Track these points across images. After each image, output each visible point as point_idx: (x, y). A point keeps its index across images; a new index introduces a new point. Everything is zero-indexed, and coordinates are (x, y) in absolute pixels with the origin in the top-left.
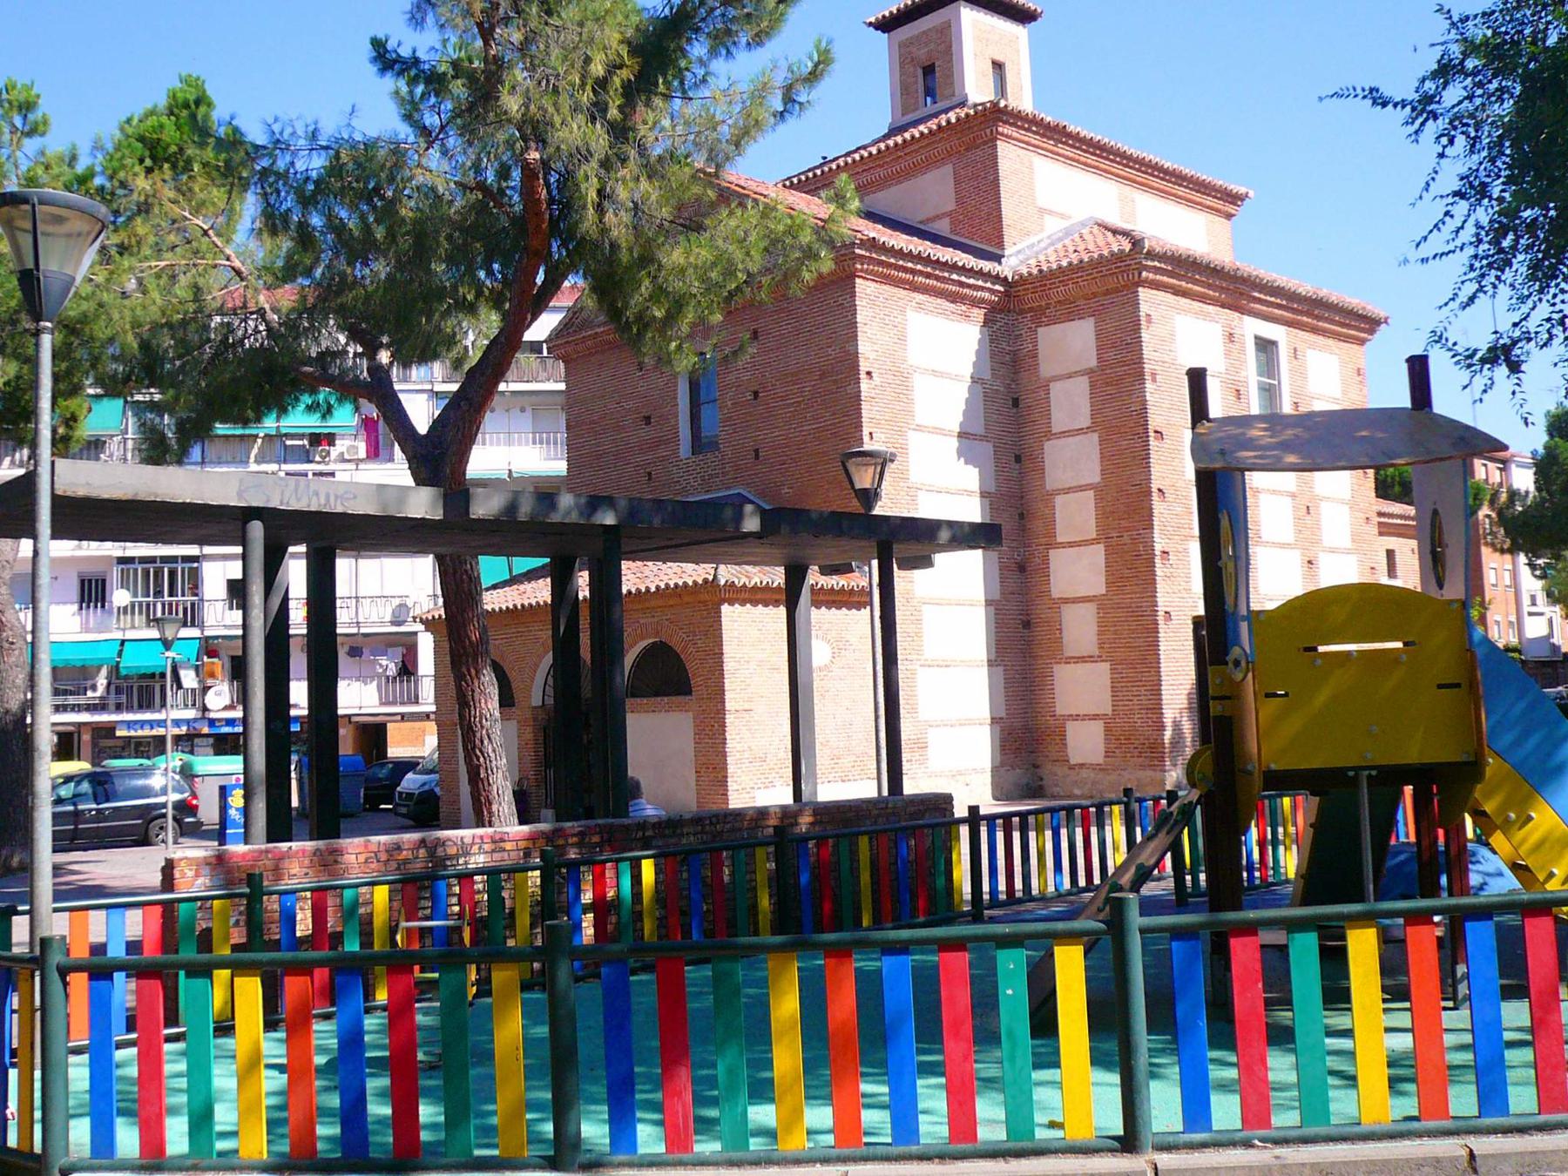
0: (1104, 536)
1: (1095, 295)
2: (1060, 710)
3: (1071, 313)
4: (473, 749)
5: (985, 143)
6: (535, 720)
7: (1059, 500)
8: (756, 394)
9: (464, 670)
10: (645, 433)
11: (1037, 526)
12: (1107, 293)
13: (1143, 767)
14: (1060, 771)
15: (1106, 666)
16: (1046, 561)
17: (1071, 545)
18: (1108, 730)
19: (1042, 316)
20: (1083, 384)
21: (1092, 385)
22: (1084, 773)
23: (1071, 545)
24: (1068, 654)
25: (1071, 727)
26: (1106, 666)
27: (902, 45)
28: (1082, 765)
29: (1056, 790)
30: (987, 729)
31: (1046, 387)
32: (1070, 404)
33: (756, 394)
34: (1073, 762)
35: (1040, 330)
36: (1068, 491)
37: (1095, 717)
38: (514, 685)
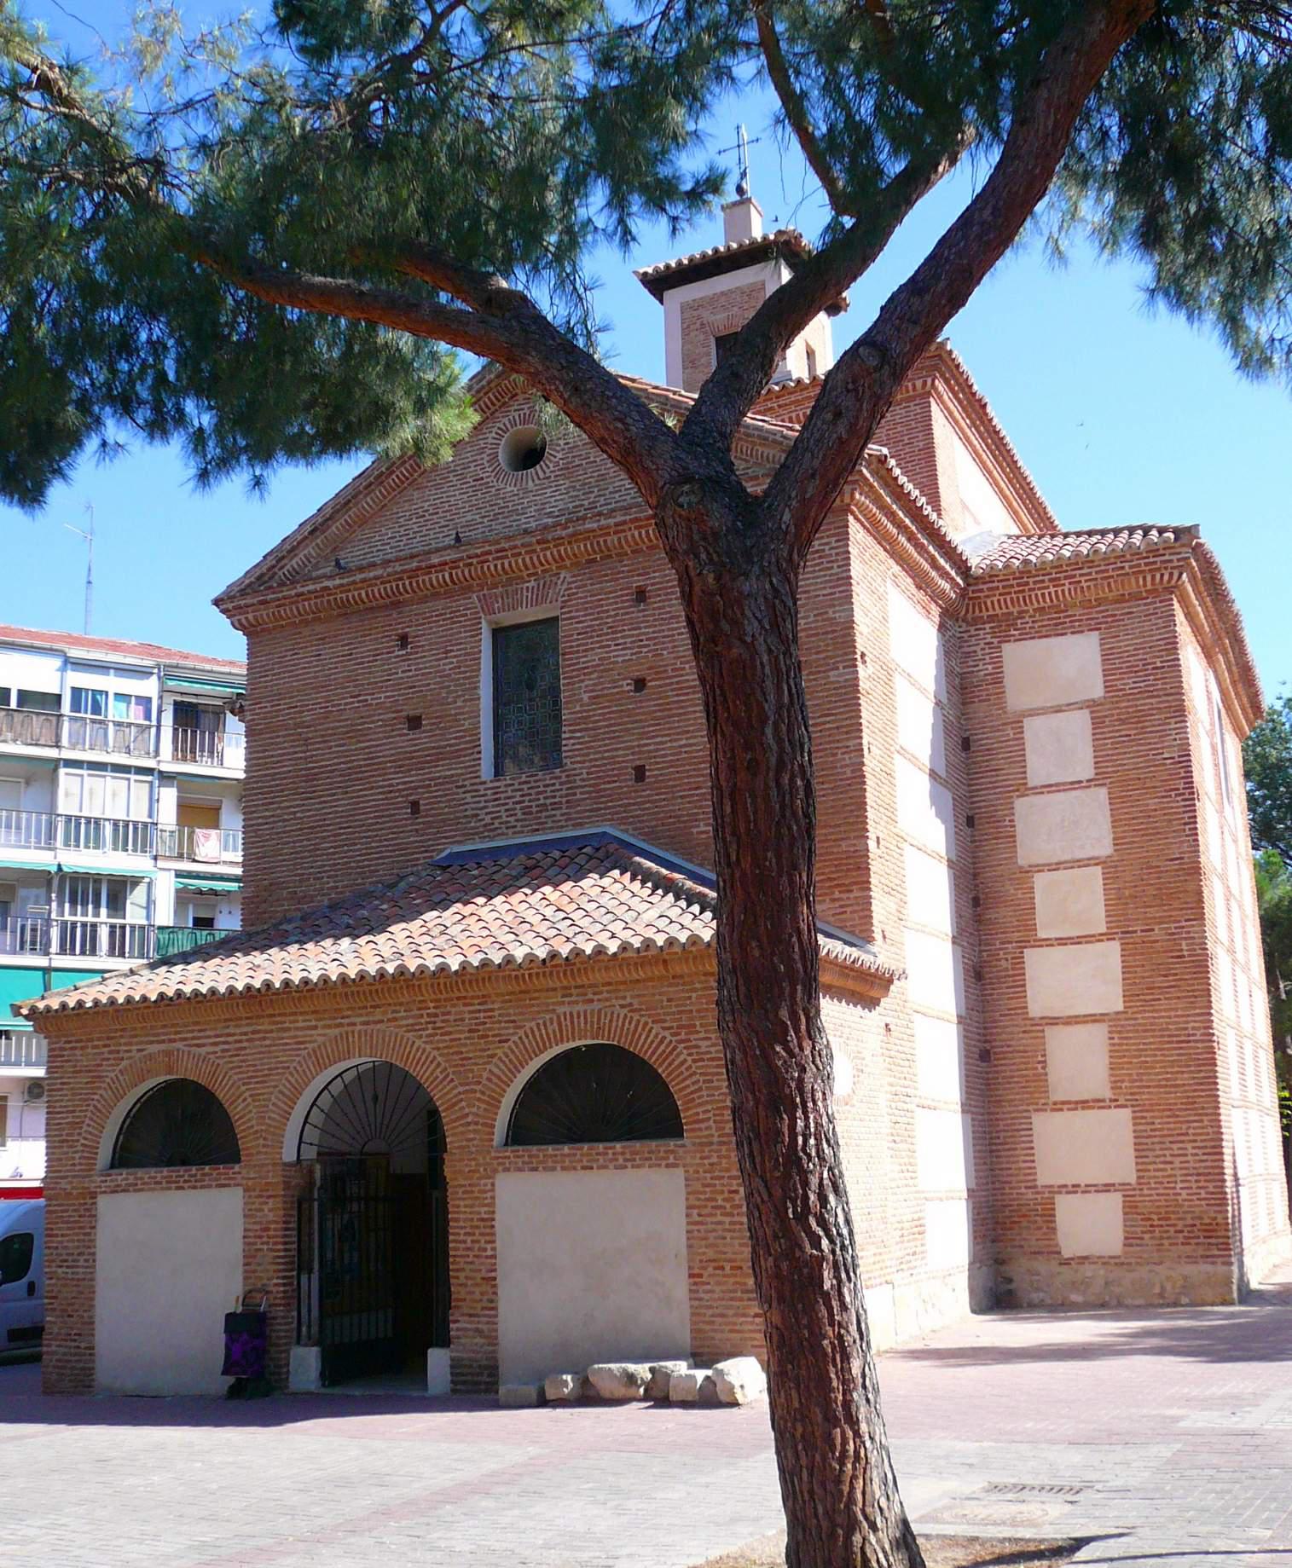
0: (1119, 927)
1: (1100, 602)
2: (1044, 1178)
3: (1058, 622)
4: (802, 1218)
5: (910, 399)
6: (287, 1185)
7: (1040, 881)
8: (640, 684)
9: (784, 1014)
10: (405, 741)
11: (1002, 915)
12: (1121, 599)
13: (1192, 1259)
14: (1042, 1266)
15: (1125, 1114)
16: (1019, 962)
17: (1062, 942)
18: (1130, 1208)
19: (1008, 627)
20: (1081, 722)
21: (1097, 723)
22: (1088, 1270)
23: (1062, 942)
24: (1057, 1095)
25: (1065, 1206)
26: (1125, 1114)
27: (685, 308)
28: (1084, 1259)
29: (1036, 1297)
30: (964, 1203)
31: (1017, 724)
32: (1058, 747)
33: (640, 684)
34: (1066, 1253)
35: (1005, 646)
36: (1056, 867)
37: (1107, 1188)
38: (239, 1128)
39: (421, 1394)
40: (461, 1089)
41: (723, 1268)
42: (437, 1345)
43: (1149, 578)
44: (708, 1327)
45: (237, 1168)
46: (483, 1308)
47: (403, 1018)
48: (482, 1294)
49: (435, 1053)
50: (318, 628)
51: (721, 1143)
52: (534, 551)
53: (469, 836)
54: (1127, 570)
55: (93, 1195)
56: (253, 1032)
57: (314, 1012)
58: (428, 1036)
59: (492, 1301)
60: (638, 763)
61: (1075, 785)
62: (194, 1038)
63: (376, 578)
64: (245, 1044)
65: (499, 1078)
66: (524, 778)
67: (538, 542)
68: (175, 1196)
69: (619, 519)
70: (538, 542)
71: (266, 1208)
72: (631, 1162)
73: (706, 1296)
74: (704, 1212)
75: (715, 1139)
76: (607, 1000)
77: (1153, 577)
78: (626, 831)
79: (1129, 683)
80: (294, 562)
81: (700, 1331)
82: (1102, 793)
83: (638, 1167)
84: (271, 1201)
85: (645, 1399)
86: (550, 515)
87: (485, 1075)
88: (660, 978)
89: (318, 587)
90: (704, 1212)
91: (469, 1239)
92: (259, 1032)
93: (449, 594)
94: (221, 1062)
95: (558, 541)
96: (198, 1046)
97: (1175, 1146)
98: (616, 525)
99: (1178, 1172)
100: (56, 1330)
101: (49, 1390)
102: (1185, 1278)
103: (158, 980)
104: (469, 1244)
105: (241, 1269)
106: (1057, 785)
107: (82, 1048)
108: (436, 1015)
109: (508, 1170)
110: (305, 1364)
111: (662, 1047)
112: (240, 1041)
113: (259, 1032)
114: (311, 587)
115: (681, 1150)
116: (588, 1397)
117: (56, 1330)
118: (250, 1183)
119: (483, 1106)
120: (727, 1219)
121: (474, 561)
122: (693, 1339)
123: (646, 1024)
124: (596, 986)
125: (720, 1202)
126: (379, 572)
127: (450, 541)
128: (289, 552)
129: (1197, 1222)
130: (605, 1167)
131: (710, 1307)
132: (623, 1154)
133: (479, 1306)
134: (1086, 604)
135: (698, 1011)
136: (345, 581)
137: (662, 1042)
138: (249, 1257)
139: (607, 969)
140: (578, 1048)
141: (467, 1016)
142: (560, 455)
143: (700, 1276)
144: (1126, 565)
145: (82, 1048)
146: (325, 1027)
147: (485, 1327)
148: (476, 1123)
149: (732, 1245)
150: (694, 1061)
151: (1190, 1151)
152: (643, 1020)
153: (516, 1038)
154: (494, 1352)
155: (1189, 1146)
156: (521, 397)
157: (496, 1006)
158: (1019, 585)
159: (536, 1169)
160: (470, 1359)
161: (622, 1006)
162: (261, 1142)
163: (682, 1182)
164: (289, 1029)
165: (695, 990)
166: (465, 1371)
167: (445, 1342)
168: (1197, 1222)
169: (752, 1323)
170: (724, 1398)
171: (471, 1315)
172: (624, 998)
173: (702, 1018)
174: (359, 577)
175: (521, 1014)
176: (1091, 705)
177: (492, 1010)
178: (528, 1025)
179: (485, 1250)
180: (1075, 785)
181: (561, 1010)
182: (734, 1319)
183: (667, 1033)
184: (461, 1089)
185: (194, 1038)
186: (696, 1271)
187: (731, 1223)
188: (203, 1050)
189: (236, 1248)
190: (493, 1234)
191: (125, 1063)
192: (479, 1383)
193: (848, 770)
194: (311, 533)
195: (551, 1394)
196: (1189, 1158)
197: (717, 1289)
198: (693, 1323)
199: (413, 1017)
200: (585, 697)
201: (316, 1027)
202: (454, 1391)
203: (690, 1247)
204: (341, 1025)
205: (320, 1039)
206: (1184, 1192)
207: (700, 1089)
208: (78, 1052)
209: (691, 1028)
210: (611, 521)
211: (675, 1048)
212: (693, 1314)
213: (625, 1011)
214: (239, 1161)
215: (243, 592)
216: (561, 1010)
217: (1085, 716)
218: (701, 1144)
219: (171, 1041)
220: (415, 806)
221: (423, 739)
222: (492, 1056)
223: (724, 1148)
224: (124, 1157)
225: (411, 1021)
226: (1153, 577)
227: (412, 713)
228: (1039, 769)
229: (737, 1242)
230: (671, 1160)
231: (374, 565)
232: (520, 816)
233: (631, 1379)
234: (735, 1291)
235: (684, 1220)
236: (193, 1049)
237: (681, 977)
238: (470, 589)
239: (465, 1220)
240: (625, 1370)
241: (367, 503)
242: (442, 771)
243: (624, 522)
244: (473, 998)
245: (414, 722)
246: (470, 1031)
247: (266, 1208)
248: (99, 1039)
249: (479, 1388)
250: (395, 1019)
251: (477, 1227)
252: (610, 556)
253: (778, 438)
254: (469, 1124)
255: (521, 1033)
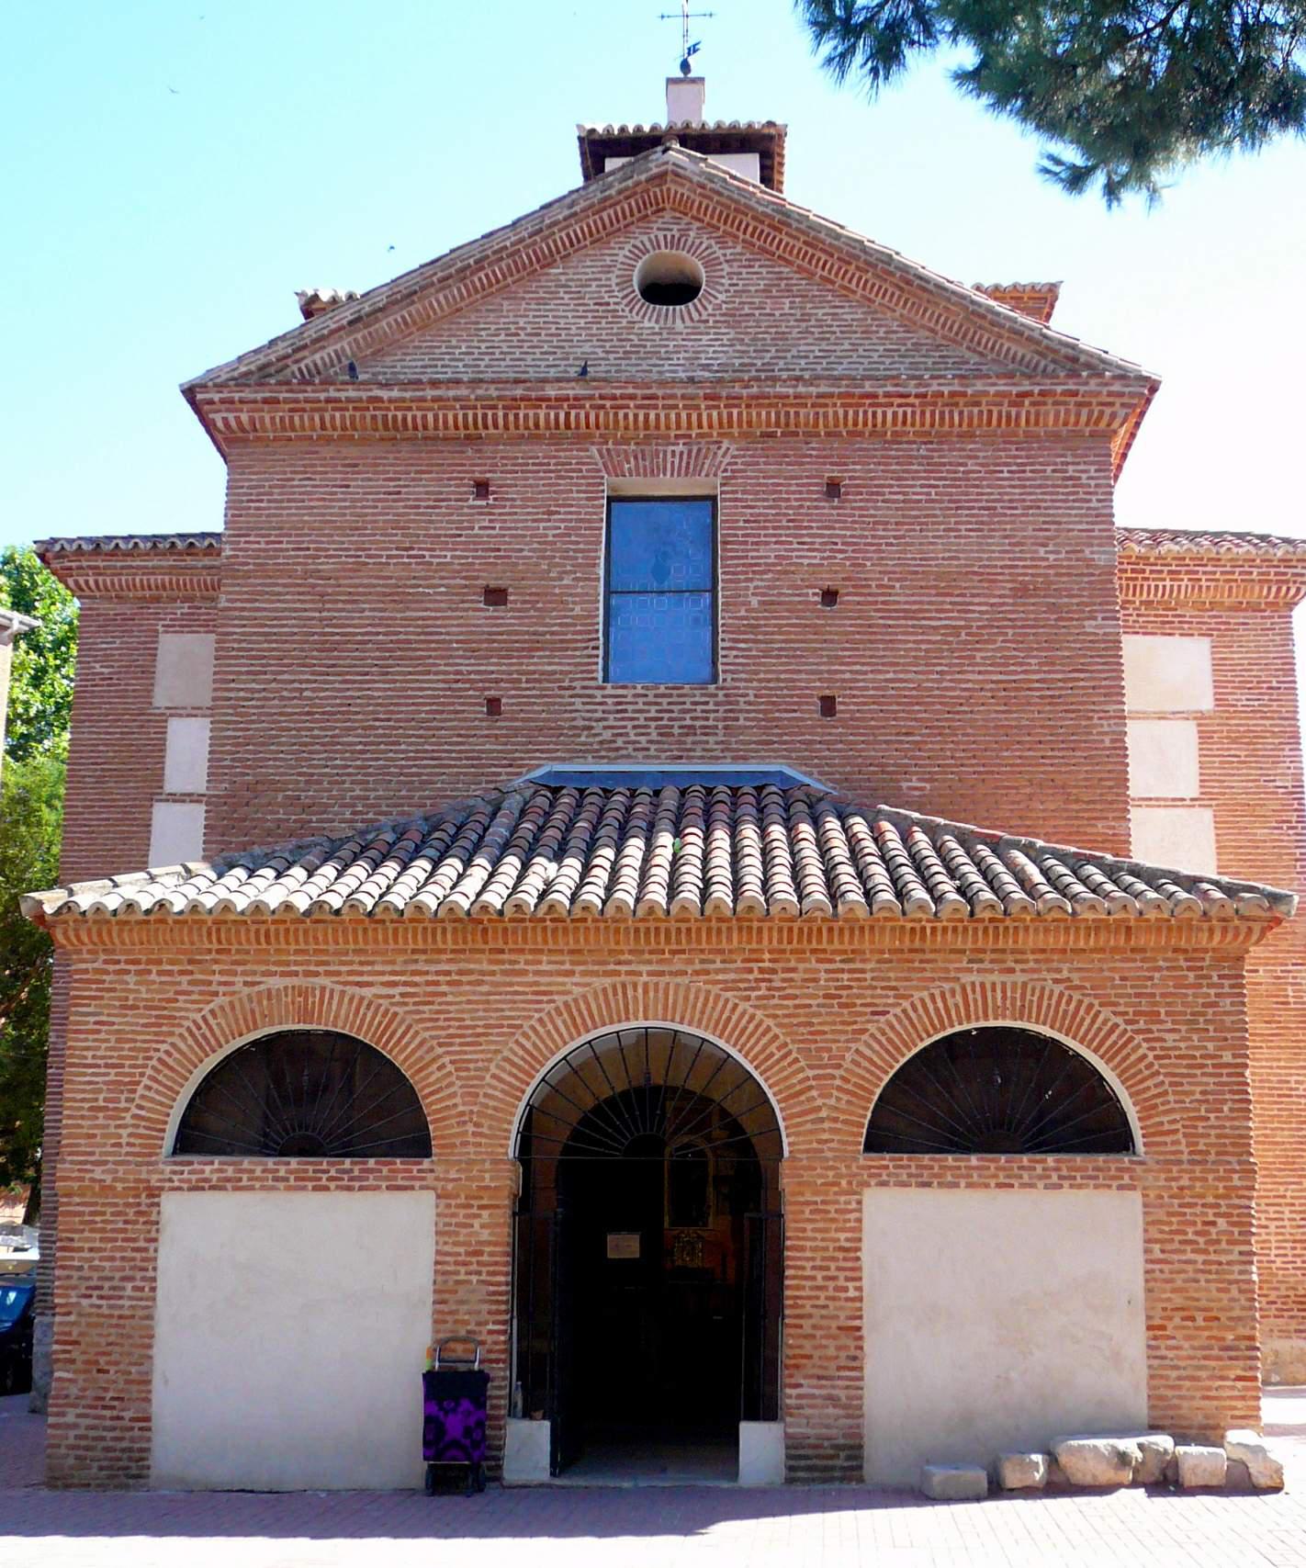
8: (830, 596)
10: (482, 616)
12: (1237, 608)
21: (1205, 737)
39: (725, 1485)
40: (810, 1073)
41: (1193, 1319)
42: (754, 1416)
43: (1274, 589)
44: (1169, 1393)
45: (426, 1163)
46: (839, 1368)
47: (718, 971)
48: (839, 1348)
49: (770, 1022)
50: (352, 452)
51: (1191, 1162)
52: (697, 407)
53: (580, 753)
54: (1254, 576)
55: (154, 1193)
56: (460, 973)
57: (571, 952)
58: (758, 998)
59: (855, 1358)
60: (827, 693)
61: (1177, 802)
62: (350, 973)
63: (456, 399)
64: (444, 988)
65: (871, 1061)
66: (662, 690)
67: (706, 397)
68: (310, 1202)
69: (823, 389)
70: (706, 397)
71: (476, 1223)
72: (1070, 1180)
73: (1170, 1354)
74: (1168, 1247)
75: (1185, 1157)
76: (1033, 971)
77: (1279, 590)
78: (810, 774)
79: (1241, 699)
80: (317, 357)
81: (1161, 1398)
82: (1207, 815)
83: (1080, 1187)
84: (485, 1213)
85: (1134, 1484)
86: (706, 367)
87: (849, 1056)
88: (1115, 950)
89: (364, 395)
90: (1168, 1247)
91: (819, 1275)
92: (470, 972)
93: (556, 440)
94: (400, 1010)
95: (734, 400)
96: (358, 984)
97: (1272, 1209)
98: (819, 396)
99: (1272, 1238)
100: (74, 1391)
101: (57, 1481)
102: (1276, 1353)
103: (222, 893)
104: (820, 1282)
105: (429, 1308)
106: (1157, 799)
107: (138, 973)
108: (774, 971)
109: (883, 1184)
110: (528, 1444)
111: (1114, 1037)
112: (437, 983)
113: (470, 972)
114: (352, 394)
115: (1139, 1168)
116: (1059, 1486)
117: (74, 1391)
118: (450, 1186)
119: (845, 1097)
120: (1200, 1258)
121: (608, 403)
122: (1152, 1407)
123: (1091, 1006)
124: (1022, 952)
125: (1190, 1236)
126: (463, 392)
127: (573, 372)
128: (315, 341)
129: (1291, 1293)
130: (1032, 1186)
131: (1176, 1368)
132: (1057, 1169)
133: (833, 1365)
134: (1199, 606)
135: (1163, 995)
136: (408, 395)
137: (1111, 1031)
138: (442, 1295)
139: (1047, 930)
140: (969, 1032)
141: (823, 975)
142: (722, 297)
143: (1163, 1328)
144: (1255, 571)
145: (138, 973)
146: (584, 974)
147: (842, 1394)
148: (835, 1120)
149: (1207, 1290)
150: (1156, 1057)
151: (1288, 1215)
152: (1086, 1001)
153: (898, 1010)
154: (858, 1426)
155: (1287, 1210)
156: (667, 215)
157: (869, 966)
158: (1133, 571)
159: (927, 1185)
160: (818, 1437)
161: (1056, 981)
162: (470, 1128)
163: (1139, 1208)
164: (524, 973)
165: (1159, 969)
166: (810, 1452)
167: (767, 1410)
168: (1291, 1293)
169: (1233, 1388)
170: (1263, 1481)
171: (820, 1378)
172: (1059, 971)
173: (1168, 1004)
174: (430, 393)
175: (907, 979)
176: (1200, 717)
177: (863, 971)
178: (917, 995)
179: (846, 1289)
180: (1177, 802)
181: (967, 979)
182: (1208, 1383)
183: (1119, 1020)
184: (810, 1073)
185: (350, 973)
186: (1157, 1322)
187: (1205, 1262)
188: (367, 992)
189: (421, 1276)
190: (859, 1269)
191: (221, 1000)
192: (833, 1468)
193: (1107, 739)
194: (351, 323)
195: (1012, 1478)
196: (1286, 1223)
197: (1186, 1345)
198: (1151, 1388)
199: (737, 971)
200: (754, 601)
201: (571, 973)
202: (790, 1481)
203: (1149, 1290)
204: (618, 973)
205: (577, 990)
206: (1279, 1260)
207: (1166, 1093)
208: (131, 979)
209: (1153, 1016)
210: (813, 390)
211: (1131, 1039)
212: (1152, 1377)
213: (1061, 987)
214: (429, 1155)
215: (241, 381)
216: (967, 979)
217: (1190, 729)
218: (1167, 1162)
219: (308, 974)
220: (494, 705)
221: (506, 617)
222: (864, 1031)
223: (1198, 1168)
224: (192, 1139)
225: (732, 976)
226: (1279, 590)
227: (493, 584)
228: (1140, 781)
229: (1213, 1286)
230: (1126, 1180)
231: (458, 382)
232: (654, 737)
233: (1123, 1458)
234: (1210, 1348)
235: (1141, 1258)
236: (350, 990)
237: (1143, 950)
238: (588, 438)
239: (814, 1249)
240: (1113, 1447)
241: (438, 300)
242: (540, 663)
243: (831, 395)
244: (835, 952)
245: (496, 596)
246: (826, 996)
247: (476, 1223)
248: (172, 962)
249: (834, 1474)
250: (707, 972)
251: (834, 1259)
252: (796, 434)
253: (1036, 334)
254: (822, 1120)
255: (906, 1004)
